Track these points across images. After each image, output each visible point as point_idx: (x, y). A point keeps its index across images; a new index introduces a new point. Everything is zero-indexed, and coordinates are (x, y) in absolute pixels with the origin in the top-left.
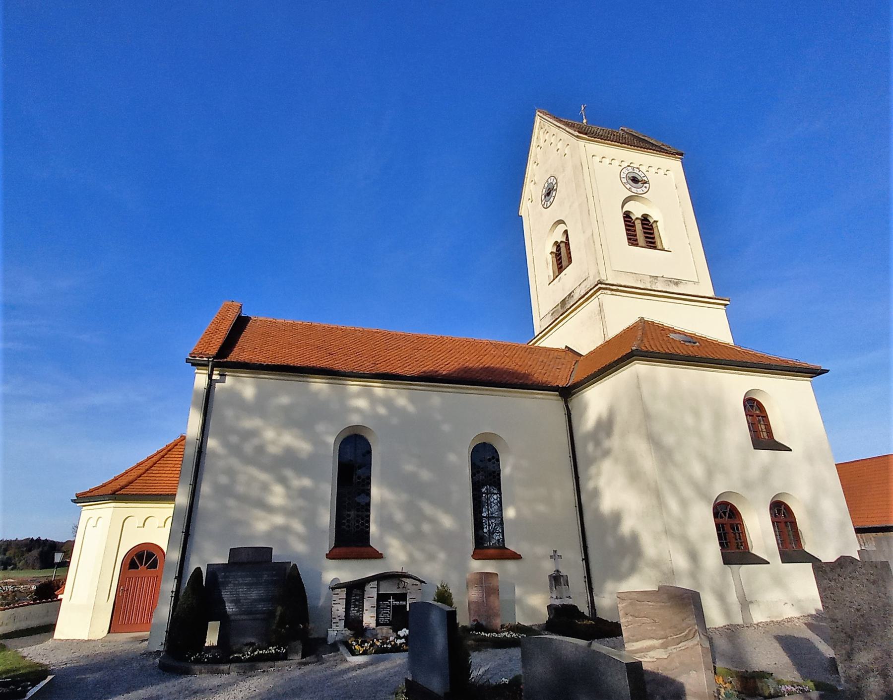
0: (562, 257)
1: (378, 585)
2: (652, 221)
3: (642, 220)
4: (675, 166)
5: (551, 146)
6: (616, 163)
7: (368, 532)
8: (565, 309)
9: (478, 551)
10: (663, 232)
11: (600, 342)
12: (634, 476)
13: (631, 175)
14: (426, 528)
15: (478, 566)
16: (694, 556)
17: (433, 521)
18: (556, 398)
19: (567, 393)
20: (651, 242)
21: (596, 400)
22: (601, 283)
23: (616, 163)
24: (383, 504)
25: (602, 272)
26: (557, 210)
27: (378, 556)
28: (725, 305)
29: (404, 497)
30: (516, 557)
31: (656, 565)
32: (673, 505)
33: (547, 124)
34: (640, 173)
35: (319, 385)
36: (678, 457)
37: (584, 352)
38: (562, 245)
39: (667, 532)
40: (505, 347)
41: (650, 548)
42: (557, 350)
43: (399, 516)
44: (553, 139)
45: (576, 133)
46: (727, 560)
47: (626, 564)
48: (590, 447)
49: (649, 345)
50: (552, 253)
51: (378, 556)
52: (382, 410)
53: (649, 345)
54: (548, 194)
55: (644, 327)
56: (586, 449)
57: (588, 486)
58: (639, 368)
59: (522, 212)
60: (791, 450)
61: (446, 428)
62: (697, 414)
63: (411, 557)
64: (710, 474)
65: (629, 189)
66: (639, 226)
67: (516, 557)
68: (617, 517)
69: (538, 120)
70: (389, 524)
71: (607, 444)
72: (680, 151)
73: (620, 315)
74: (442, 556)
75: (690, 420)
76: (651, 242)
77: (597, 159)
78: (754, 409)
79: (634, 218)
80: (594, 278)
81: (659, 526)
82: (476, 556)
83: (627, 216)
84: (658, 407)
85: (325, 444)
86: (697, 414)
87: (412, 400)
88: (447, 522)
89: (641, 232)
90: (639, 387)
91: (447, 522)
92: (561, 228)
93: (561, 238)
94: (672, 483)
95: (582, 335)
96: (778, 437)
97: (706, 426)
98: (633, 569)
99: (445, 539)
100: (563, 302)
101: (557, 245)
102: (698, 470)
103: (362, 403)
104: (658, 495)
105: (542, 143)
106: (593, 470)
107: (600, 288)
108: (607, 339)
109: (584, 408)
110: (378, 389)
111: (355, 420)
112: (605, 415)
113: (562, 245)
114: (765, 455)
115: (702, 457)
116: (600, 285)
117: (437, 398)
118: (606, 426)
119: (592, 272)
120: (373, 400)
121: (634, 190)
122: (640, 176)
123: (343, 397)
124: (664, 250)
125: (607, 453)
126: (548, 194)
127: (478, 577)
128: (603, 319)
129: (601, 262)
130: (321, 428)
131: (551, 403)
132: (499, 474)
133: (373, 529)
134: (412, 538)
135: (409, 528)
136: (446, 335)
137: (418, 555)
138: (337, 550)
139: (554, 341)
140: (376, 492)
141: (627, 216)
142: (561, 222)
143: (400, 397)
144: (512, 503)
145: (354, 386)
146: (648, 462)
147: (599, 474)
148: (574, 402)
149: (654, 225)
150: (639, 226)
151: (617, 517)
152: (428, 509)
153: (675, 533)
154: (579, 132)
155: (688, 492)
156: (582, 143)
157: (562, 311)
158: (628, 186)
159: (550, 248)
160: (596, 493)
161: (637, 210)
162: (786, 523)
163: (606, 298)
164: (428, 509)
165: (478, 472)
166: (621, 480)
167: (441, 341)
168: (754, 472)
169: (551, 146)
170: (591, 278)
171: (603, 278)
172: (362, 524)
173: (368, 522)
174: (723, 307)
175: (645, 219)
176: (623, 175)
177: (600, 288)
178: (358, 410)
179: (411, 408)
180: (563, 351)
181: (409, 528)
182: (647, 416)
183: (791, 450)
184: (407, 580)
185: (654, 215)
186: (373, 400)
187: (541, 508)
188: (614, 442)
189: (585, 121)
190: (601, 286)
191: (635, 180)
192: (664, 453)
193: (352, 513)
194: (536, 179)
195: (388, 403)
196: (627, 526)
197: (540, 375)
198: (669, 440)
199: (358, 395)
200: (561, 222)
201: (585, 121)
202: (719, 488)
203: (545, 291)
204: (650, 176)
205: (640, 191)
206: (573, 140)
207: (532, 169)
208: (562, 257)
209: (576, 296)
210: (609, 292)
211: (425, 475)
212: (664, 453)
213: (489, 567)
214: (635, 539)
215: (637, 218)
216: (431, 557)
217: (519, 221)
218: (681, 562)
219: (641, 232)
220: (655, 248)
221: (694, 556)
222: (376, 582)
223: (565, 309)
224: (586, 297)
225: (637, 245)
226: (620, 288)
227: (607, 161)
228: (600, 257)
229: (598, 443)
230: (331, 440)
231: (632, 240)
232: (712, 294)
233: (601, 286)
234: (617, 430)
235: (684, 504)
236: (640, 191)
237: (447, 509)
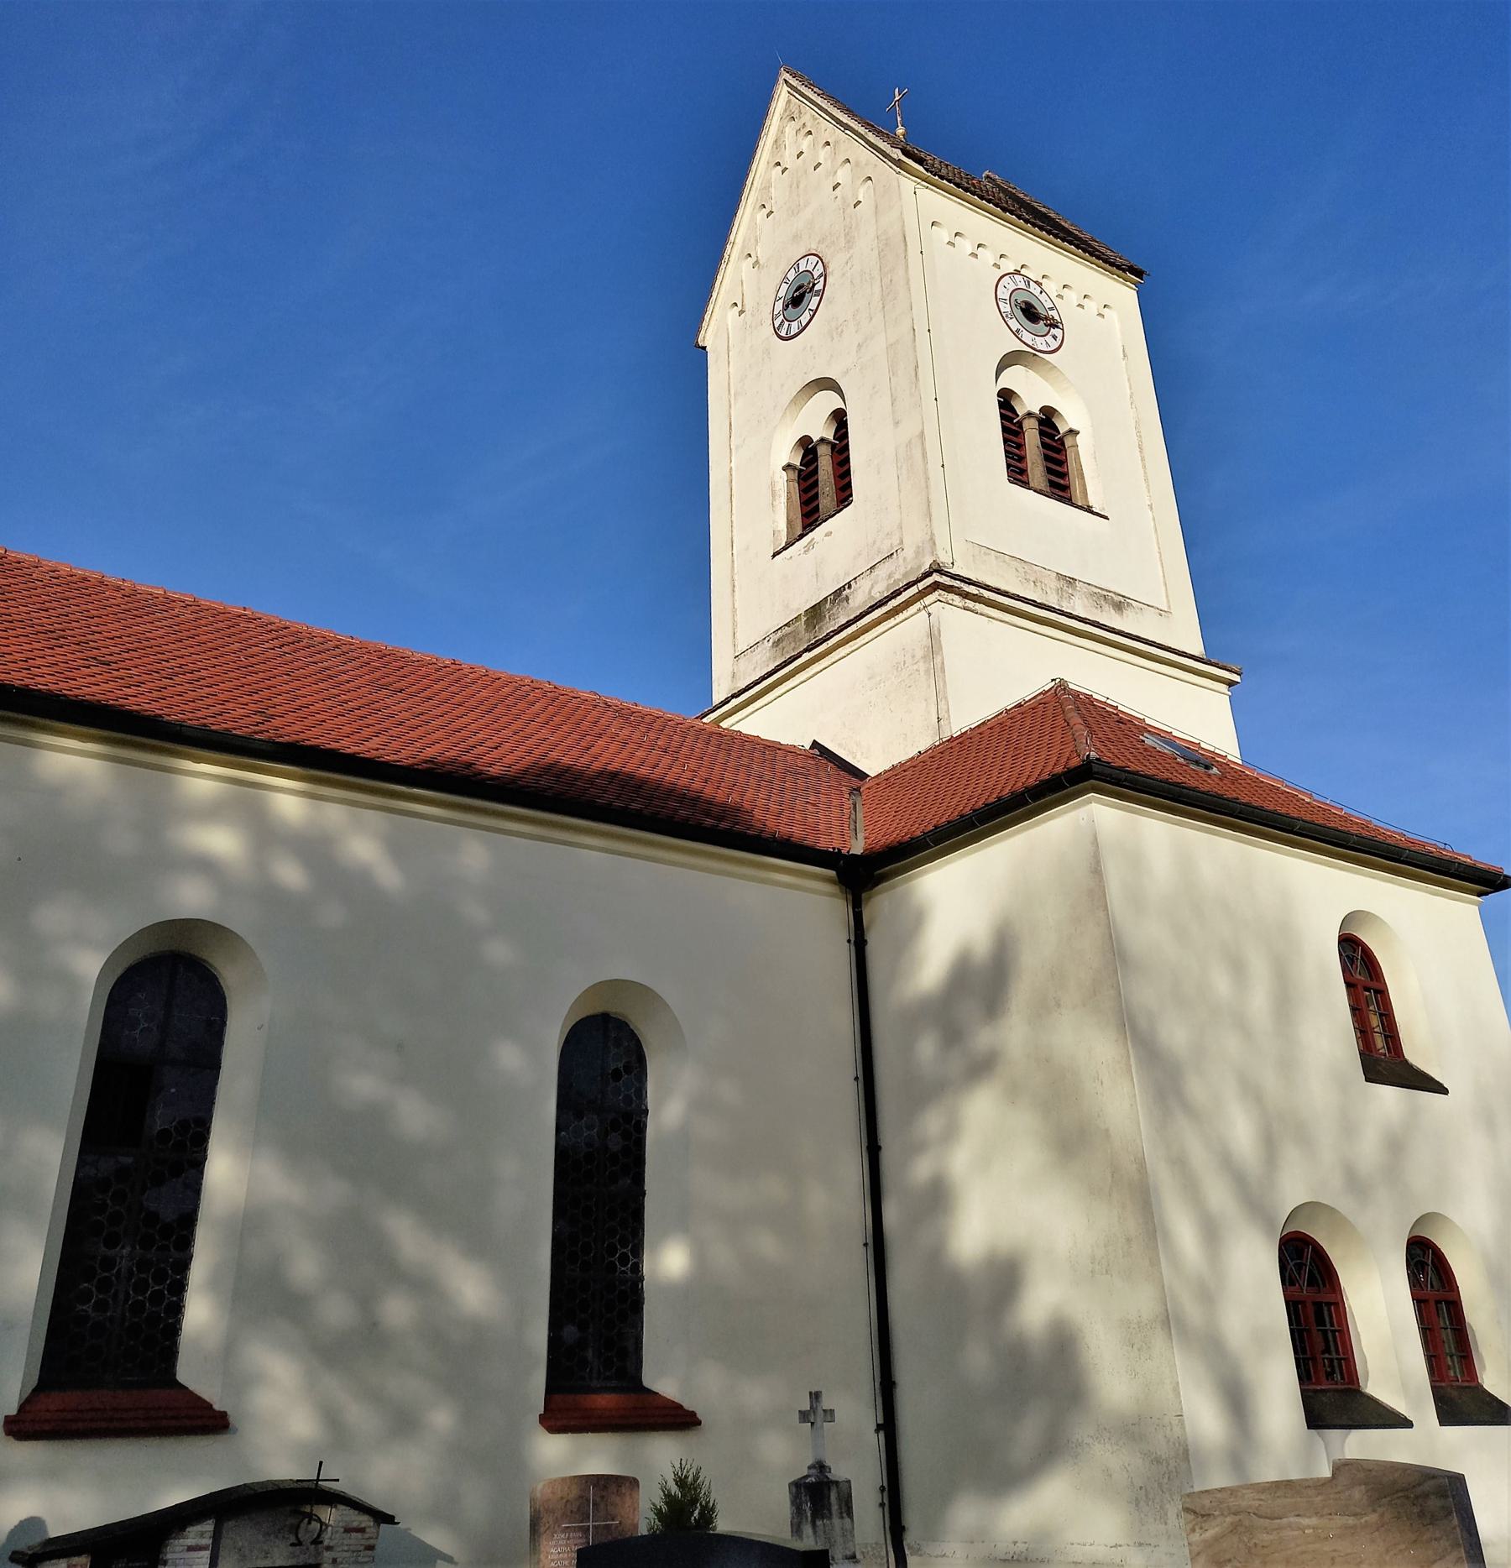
0: (820, 481)
1: (217, 1536)
2: (1062, 429)
3: (1041, 422)
4: (1122, 296)
5: (810, 175)
6: (988, 257)
7: (174, 1330)
8: (817, 632)
9: (557, 1398)
10: (1089, 458)
11: (923, 742)
12: (1071, 1140)
13: (1022, 297)
14: (397, 1311)
15: (561, 1457)
16: (1237, 1400)
17: (423, 1286)
18: (829, 880)
19: (861, 876)
20: (1060, 483)
21: (955, 901)
22: (940, 571)
23: (988, 257)
24: (250, 1224)
25: (942, 542)
26: (815, 350)
27: (207, 1422)
28: (1231, 684)
29: (335, 1191)
30: (679, 1419)
31: (1132, 1430)
32: (1185, 1234)
33: (808, 115)
34: (1043, 297)
35: (71, 762)
36: (1196, 1089)
37: (872, 766)
38: (824, 452)
39: (1169, 1321)
40: (651, 722)
41: (1114, 1379)
42: (790, 751)
43: (306, 1267)
44: (823, 155)
45: (897, 154)
46: (1317, 1416)
47: (1028, 1432)
48: (927, 1047)
49: (1060, 758)
50: (788, 467)
51: (207, 1422)
52: (290, 874)
53: (1060, 758)
54: (796, 301)
55: (1059, 705)
56: (908, 1054)
57: (909, 1172)
58: (1097, 814)
59: (709, 337)
60: (1445, 1091)
61: (499, 952)
62: (1238, 968)
63: (332, 1419)
64: (1269, 1143)
65: (1016, 333)
66: (1032, 437)
67: (679, 1419)
68: (1005, 1277)
69: (782, 95)
70: (263, 1296)
71: (983, 1038)
72: (1140, 266)
73: (993, 671)
74: (442, 1419)
75: (1221, 984)
76: (1060, 483)
77: (944, 235)
78: (1359, 963)
79: (1021, 412)
80: (919, 552)
81: (1141, 1302)
82: (557, 1419)
83: (1006, 399)
84: (1147, 934)
85: (66, 979)
86: (1238, 968)
87: (396, 849)
88: (471, 1289)
89: (1041, 454)
90: (1097, 870)
91: (471, 1289)
92: (828, 401)
93: (820, 429)
94: (1180, 1163)
95: (870, 713)
96: (1416, 1052)
97: (1259, 1002)
98: (1052, 1450)
99: (457, 1354)
100: (815, 613)
101: (807, 447)
102: (1242, 1132)
103: (221, 842)
104: (1142, 1200)
105: (788, 159)
106: (932, 1122)
107: (936, 586)
108: (946, 736)
109: (914, 923)
110: (288, 798)
111: (191, 899)
112: (982, 943)
113: (824, 452)
114: (1389, 1096)
115: (1251, 1092)
116: (936, 577)
117: (480, 851)
118: (984, 981)
119: (913, 538)
120: (264, 833)
121: (1027, 337)
122: (1043, 304)
123: (157, 816)
124: (1089, 510)
125: (982, 1067)
126: (796, 301)
127: (575, 1492)
128: (937, 673)
129: (938, 512)
130: (54, 916)
131: (805, 905)
132: (641, 1128)
133: (200, 1312)
134: (345, 1352)
135: (336, 1312)
136: (466, 660)
137: (358, 1415)
138: (55, 1401)
139: (782, 720)
140: (225, 1172)
141: (1006, 399)
142: (827, 384)
143: (362, 835)
144: (682, 1224)
145: (202, 779)
146: (1119, 1102)
147: (951, 1133)
148: (881, 904)
149: (1068, 442)
150: (1032, 437)
151: (1005, 1277)
152: (408, 1236)
153: (1183, 1324)
154: (906, 153)
155: (1219, 1195)
156: (908, 183)
157: (807, 639)
158: (1014, 325)
159: (786, 452)
160: (938, 1198)
161: (1033, 395)
162: (1438, 1302)
163: (947, 613)
164: (408, 1236)
165: (579, 1115)
166: (1027, 1154)
167: (453, 674)
168: (1368, 1150)
169: (810, 175)
170: (909, 552)
171: (944, 559)
172: (157, 1298)
173: (180, 1287)
174: (1223, 688)
175: (1047, 419)
176: (1004, 294)
177: (936, 586)
178: (205, 866)
179: (388, 876)
180: (805, 755)
181: (336, 1312)
182: (1116, 956)
183: (1445, 1091)
184: (330, 1515)
185: (1071, 416)
186: (264, 833)
187: (767, 1245)
188: (1013, 1034)
189: (900, 131)
190: (939, 581)
191: (1030, 313)
192: (1164, 1078)
193: (124, 1253)
194: (761, 252)
195: (313, 849)
196: (1040, 1304)
197: (769, 812)
198: (1175, 1035)
199: (212, 812)
200: (827, 384)
201: (900, 131)
202: (1292, 1192)
203: (755, 572)
204: (1066, 310)
205: (1040, 343)
206: (884, 170)
207: (753, 218)
208: (820, 481)
209: (859, 599)
210: (957, 600)
211: (416, 1116)
212: (1164, 1078)
213: (596, 1455)
214: (1063, 1344)
215: (1030, 414)
216: (403, 1423)
217: (693, 365)
218: (1205, 1419)
219: (1041, 454)
220: (1068, 501)
221: (1237, 1400)
222: (208, 1526)
223: (817, 632)
224: (890, 605)
225: (1025, 484)
226: (987, 594)
227: (967, 246)
228: (937, 496)
229: (952, 1036)
230: (89, 966)
231: (1017, 473)
232: (1197, 649)
233: (939, 581)
234: (1021, 995)
235: (1211, 1233)
236: (1040, 343)
237: (478, 1241)
